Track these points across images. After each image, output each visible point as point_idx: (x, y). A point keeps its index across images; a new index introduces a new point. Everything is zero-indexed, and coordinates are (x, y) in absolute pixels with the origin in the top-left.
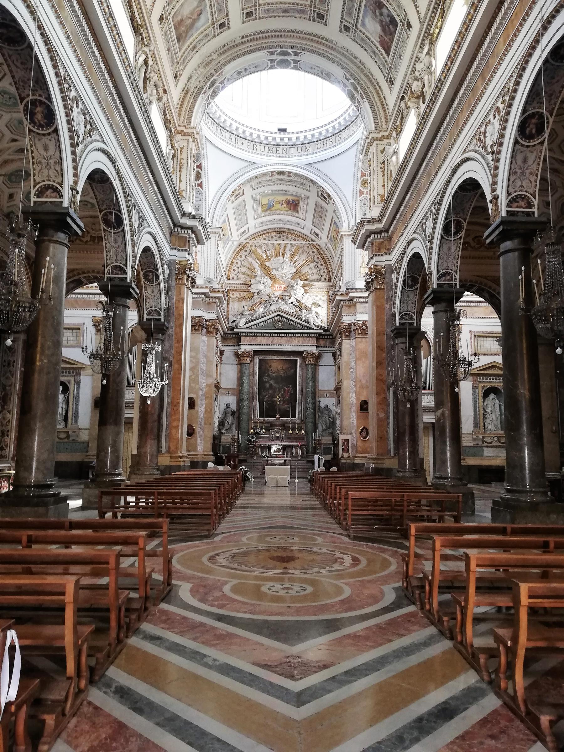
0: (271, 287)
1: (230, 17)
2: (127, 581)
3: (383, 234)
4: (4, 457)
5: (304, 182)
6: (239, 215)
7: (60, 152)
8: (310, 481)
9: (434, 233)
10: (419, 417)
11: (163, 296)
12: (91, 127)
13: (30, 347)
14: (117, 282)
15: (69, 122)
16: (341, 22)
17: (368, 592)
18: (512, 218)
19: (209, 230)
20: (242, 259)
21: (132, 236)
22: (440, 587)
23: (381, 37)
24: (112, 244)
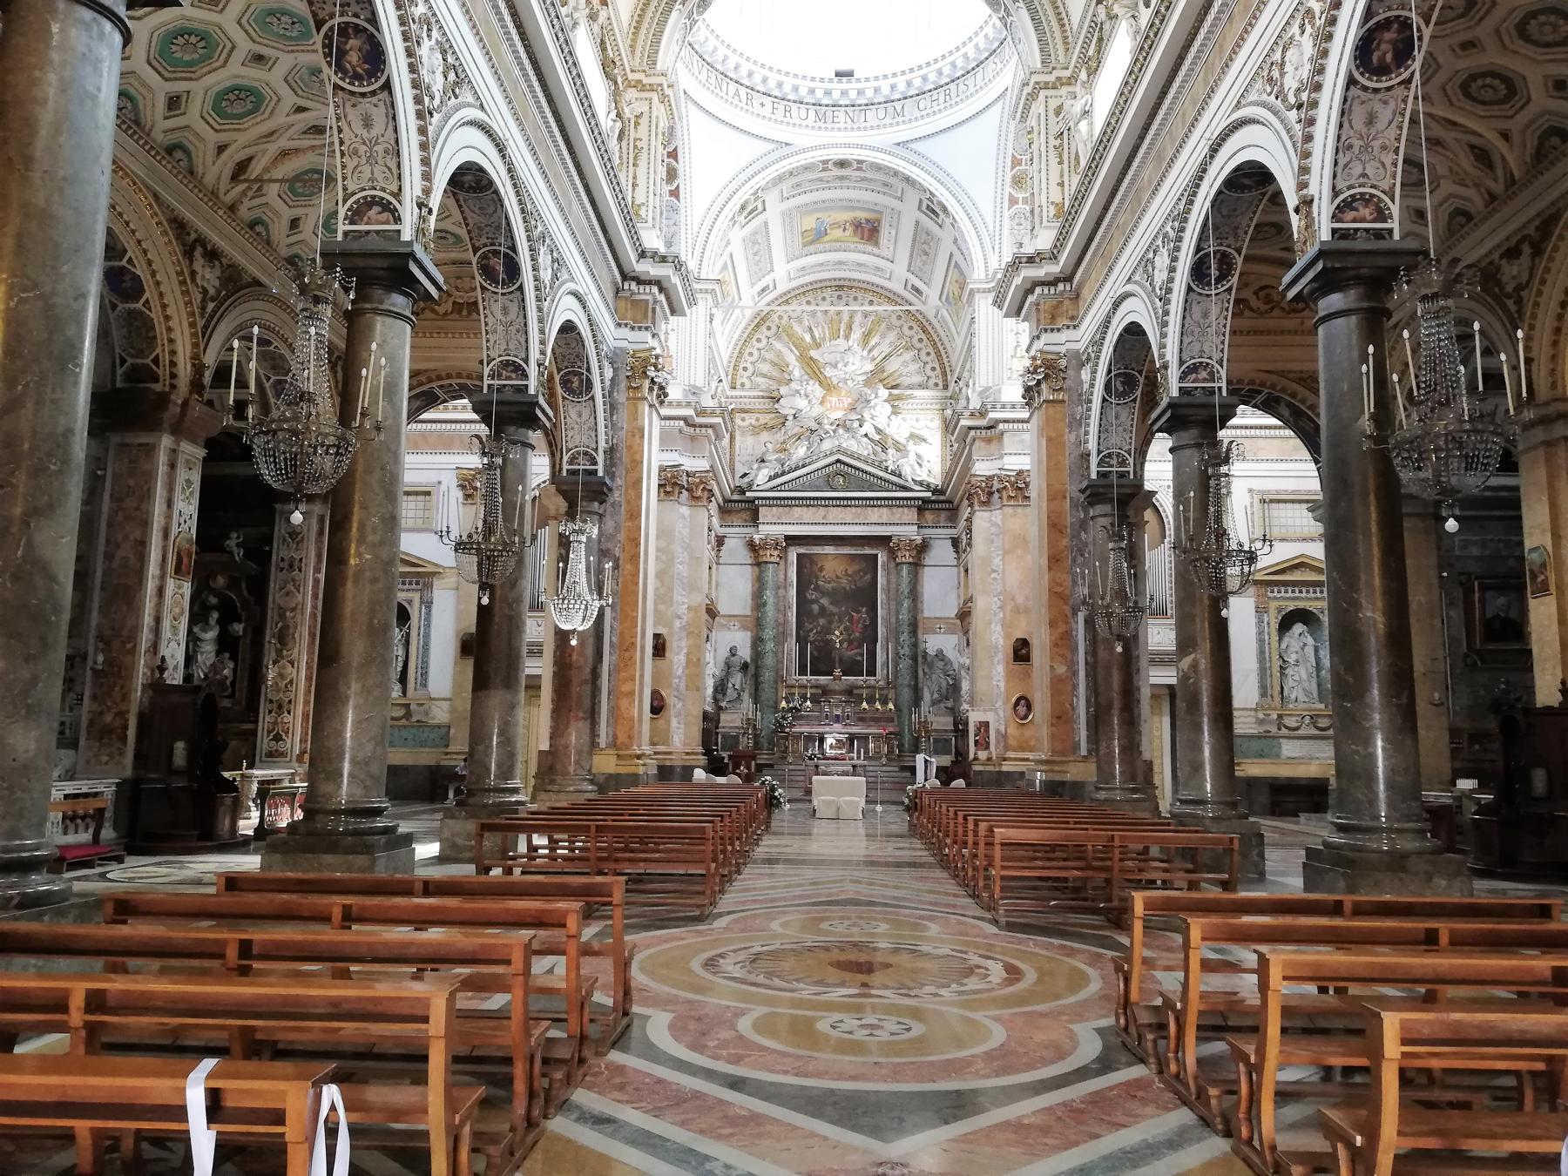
0: (822, 403)
2: (537, 1004)
3: (1061, 286)
4: (283, 754)
5: (891, 180)
6: (756, 254)
7: (396, 130)
8: (908, 809)
9: (1171, 280)
10: (1142, 672)
11: (601, 423)
12: (458, 79)
13: (339, 525)
14: (509, 395)
15: (413, 69)
17: (1043, 1037)
18: (1343, 245)
19: (695, 286)
20: (761, 345)
21: (538, 299)
22: (1199, 1028)
24: (499, 316)
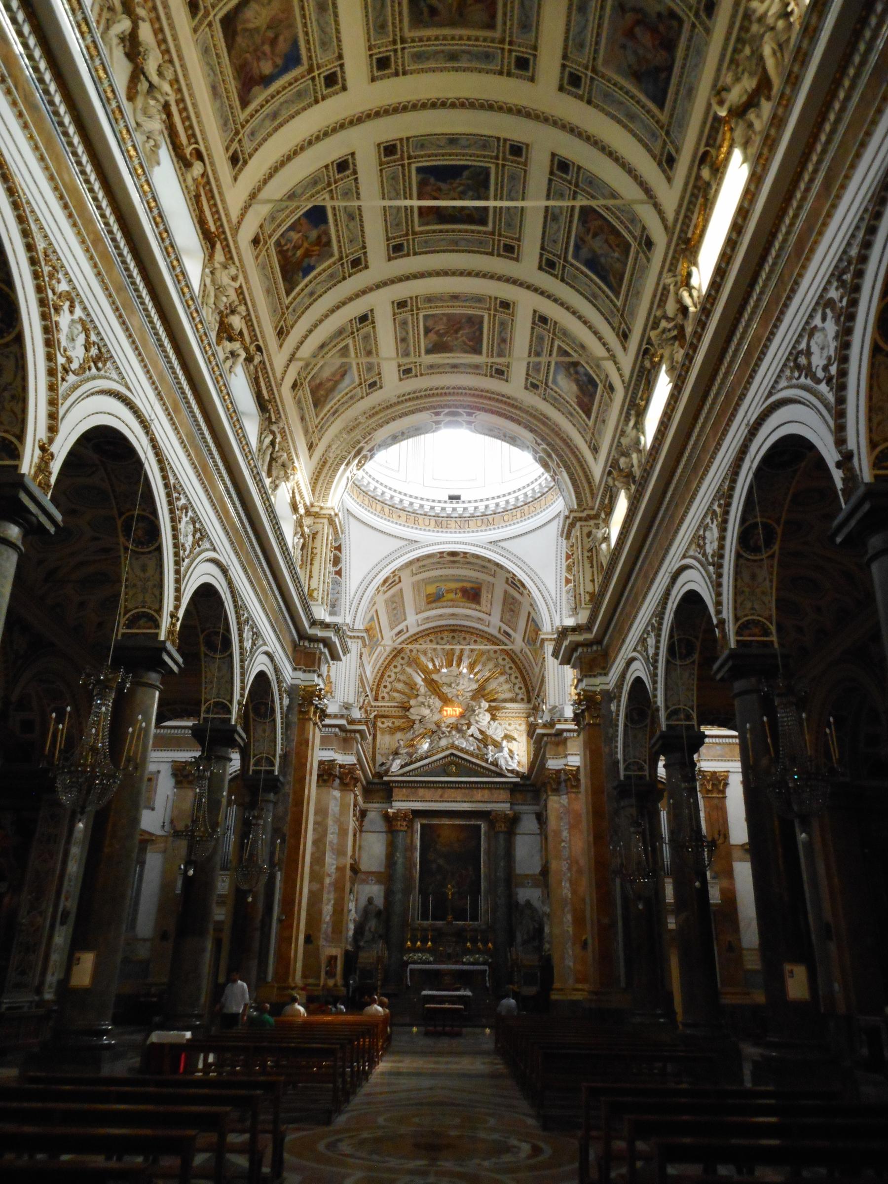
1: (359, 175)
3: (595, 648)
12: (201, 535)
16: (541, 255)
20: (397, 670)
23: (577, 397)
